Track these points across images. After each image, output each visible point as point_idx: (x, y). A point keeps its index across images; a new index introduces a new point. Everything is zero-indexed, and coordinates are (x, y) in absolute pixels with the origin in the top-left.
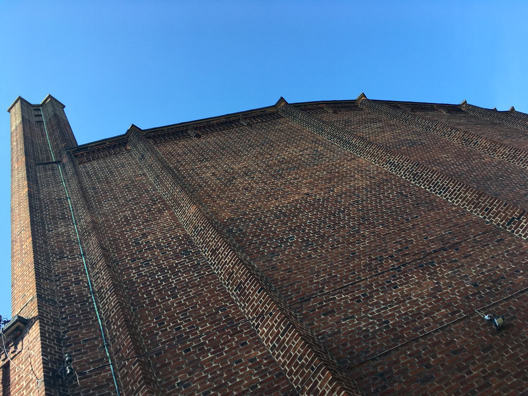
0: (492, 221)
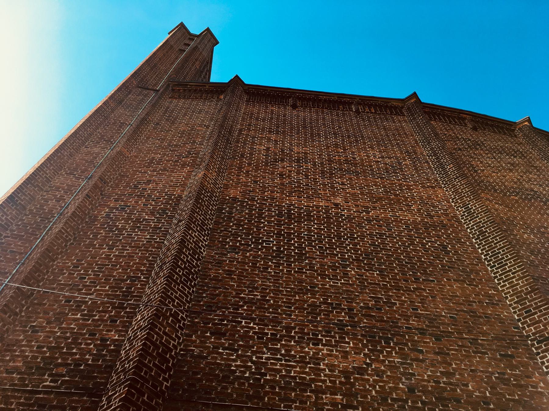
0: (524, 328)
